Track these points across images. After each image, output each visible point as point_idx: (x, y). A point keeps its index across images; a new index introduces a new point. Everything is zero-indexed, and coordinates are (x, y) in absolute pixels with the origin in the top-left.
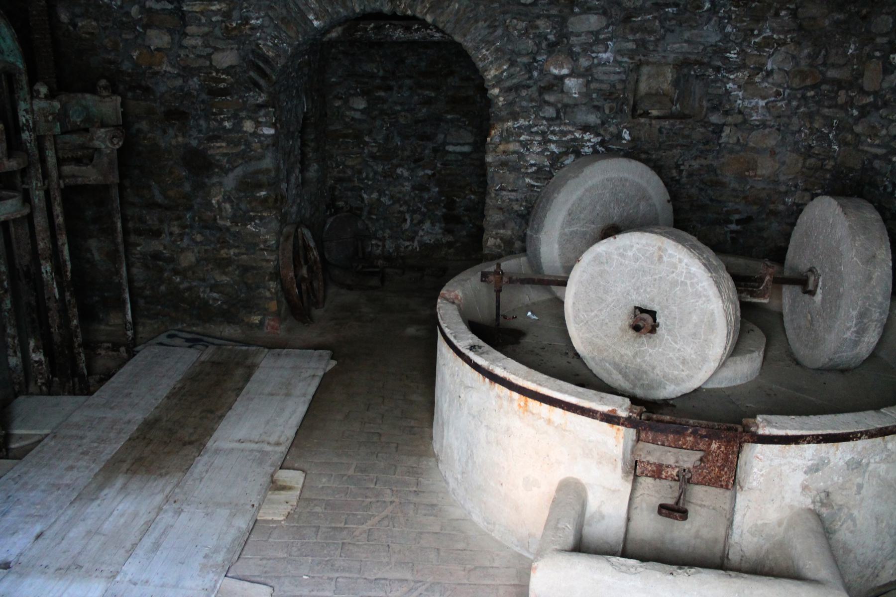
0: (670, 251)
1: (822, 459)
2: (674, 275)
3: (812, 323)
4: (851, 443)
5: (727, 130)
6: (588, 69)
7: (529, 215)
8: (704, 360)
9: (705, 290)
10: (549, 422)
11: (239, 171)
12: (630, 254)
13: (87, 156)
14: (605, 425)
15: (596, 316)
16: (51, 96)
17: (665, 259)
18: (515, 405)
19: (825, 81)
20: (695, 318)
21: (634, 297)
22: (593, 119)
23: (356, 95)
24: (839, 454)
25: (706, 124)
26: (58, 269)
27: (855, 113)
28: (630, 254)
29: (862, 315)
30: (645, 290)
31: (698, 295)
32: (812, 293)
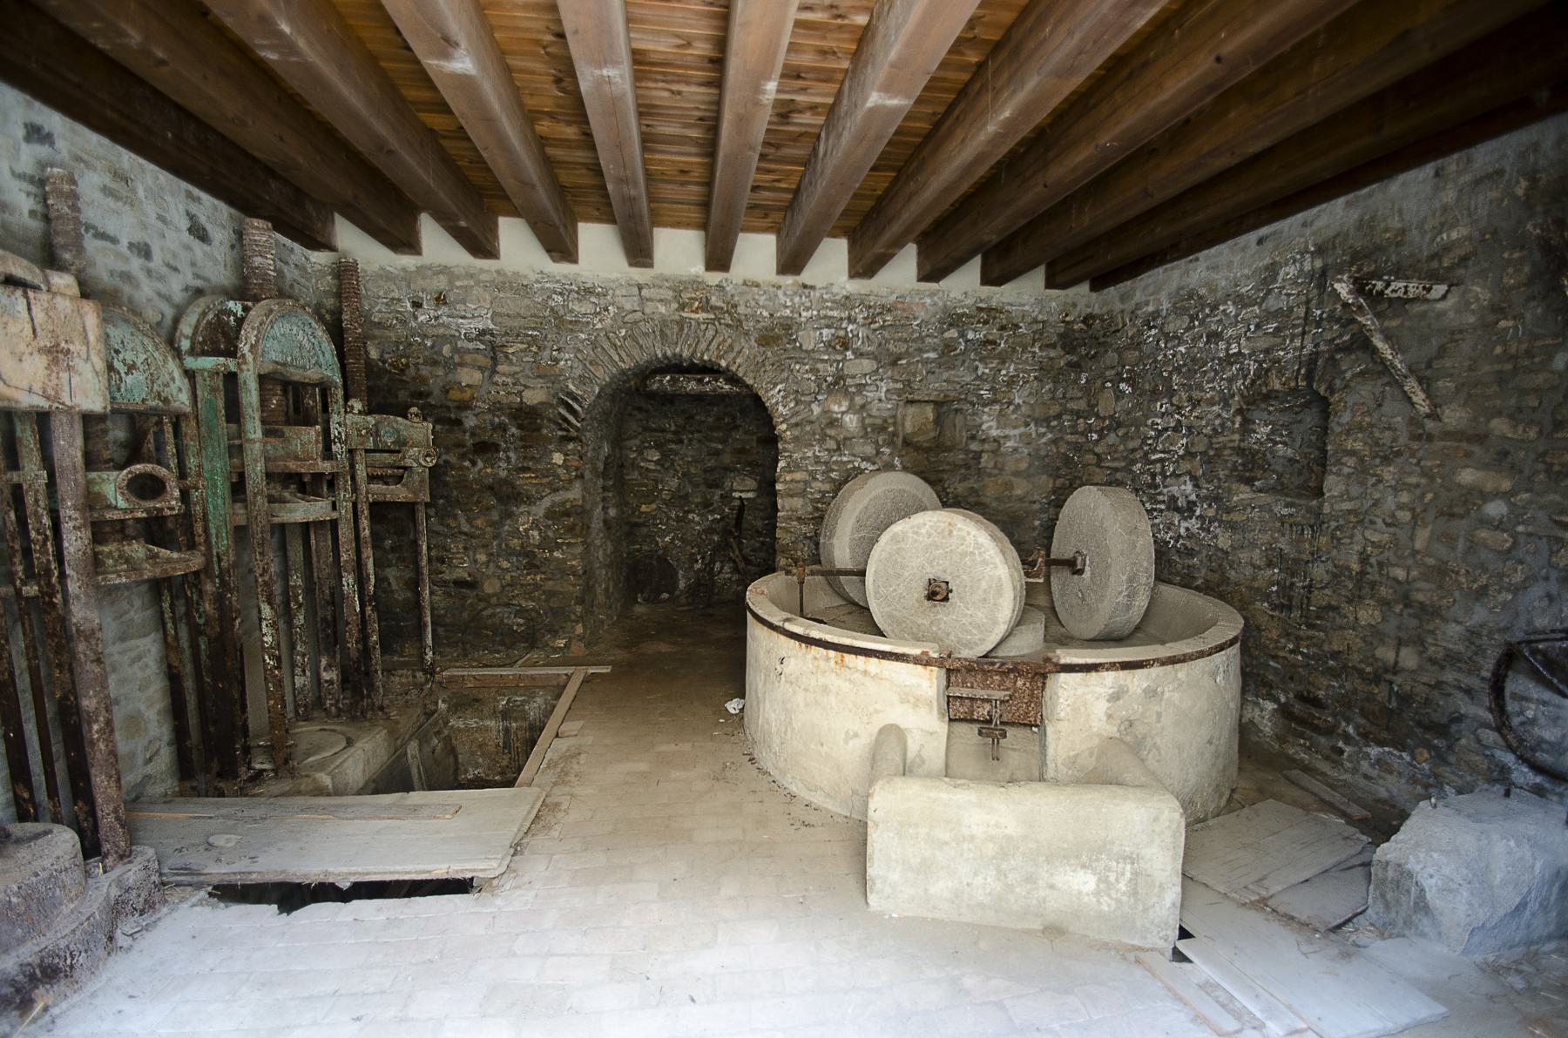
1: (1121, 687)
3: (1083, 599)
4: (1145, 671)
5: (985, 457)
6: (863, 407)
7: (819, 517)
8: (995, 623)
10: (865, 673)
11: (547, 502)
12: (923, 531)
13: (399, 475)
16: (369, 411)
19: (1065, 411)
20: (984, 584)
22: (869, 450)
23: (650, 447)
24: (1136, 681)
25: (967, 452)
26: (361, 581)
27: (1095, 437)
28: (923, 531)
29: (1131, 580)
31: (985, 563)
32: (1080, 572)
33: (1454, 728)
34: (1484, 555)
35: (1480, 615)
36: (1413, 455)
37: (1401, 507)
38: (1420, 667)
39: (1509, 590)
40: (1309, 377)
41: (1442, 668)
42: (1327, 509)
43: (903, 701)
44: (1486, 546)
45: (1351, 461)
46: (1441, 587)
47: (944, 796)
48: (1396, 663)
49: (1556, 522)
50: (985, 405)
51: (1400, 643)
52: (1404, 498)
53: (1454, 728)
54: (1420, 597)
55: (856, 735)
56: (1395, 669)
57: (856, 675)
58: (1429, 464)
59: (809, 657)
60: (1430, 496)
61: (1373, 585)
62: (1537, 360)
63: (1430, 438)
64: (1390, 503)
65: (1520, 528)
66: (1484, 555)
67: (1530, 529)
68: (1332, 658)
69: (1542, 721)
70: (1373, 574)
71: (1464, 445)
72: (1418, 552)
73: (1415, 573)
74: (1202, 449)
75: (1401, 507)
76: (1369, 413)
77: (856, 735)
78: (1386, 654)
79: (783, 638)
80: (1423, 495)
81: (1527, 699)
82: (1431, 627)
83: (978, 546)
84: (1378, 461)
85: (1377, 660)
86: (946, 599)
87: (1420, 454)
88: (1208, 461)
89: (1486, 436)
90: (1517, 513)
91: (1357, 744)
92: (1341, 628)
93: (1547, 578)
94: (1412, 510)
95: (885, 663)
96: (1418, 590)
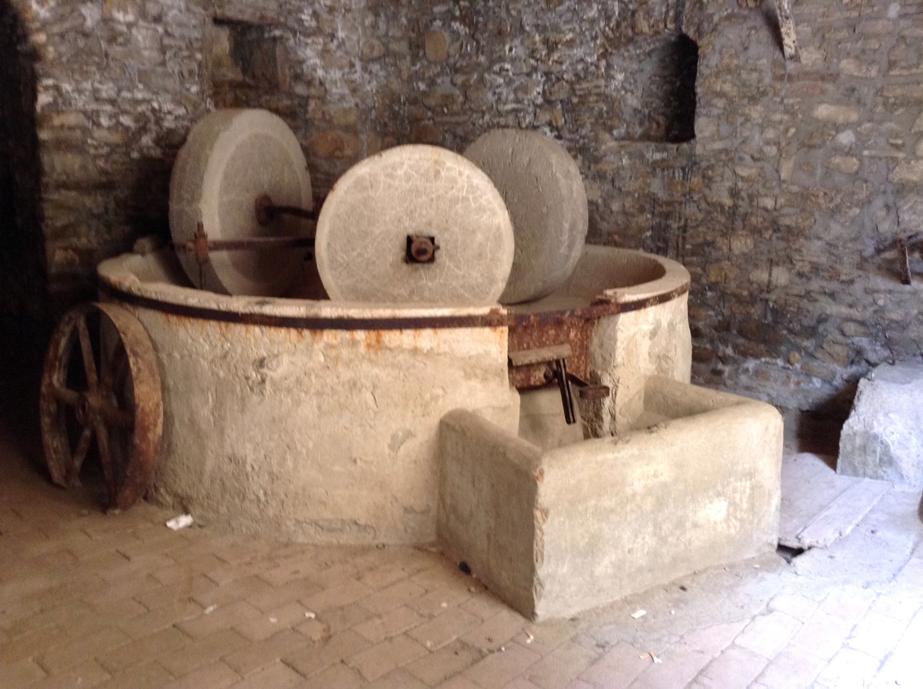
0: (448, 164)
2: (454, 191)
5: (312, 104)
8: (492, 281)
9: (489, 202)
14: (487, 330)
15: (360, 255)
17: (443, 174)
18: (362, 349)
21: (407, 224)
25: (291, 95)
28: (400, 172)
30: (421, 214)
31: (481, 210)
33: (821, 328)
34: (838, 178)
35: (836, 229)
36: (776, 94)
37: (767, 143)
38: (791, 282)
39: (857, 206)
40: (677, 19)
41: (809, 279)
42: (699, 150)
43: (468, 376)
44: (840, 172)
45: (721, 103)
46: (803, 210)
47: (610, 456)
48: (770, 282)
49: (892, 145)
50: (307, 35)
51: (772, 263)
52: (770, 134)
53: (821, 328)
54: (787, 221)
55: (409, 434)
56: (769, 287)
57: (401, 357)
58: (791, 101)
59: (319, 346)
60: (792, 130)
61: (745, 216)
62: (876, 9)
63: (790, 78)
64: (757, 139)
65: (866, 153)
66: (838, 178)
67: (874, 153)
68: (710, 289)
69: (890, 306)
70: (744, 207)
71: (820, 83)
72: (784, 181)
73: (781, 201)
74: (563, 95)
75: (767, 143)
76: (737, 55)
77: (409, 434)
78: (760, 276)
79: (256, 330)
80: (787, 130)
81: (877, 291)
82: (797, 246)
83: (472, 188)
84: (746, 101)
85: (751, 283)
86: (432, 260)
87: (783, 93)
88: (569, 108)
89: (838, 75)
90: (862, 141)
91: (735, 361)
92: (718, 260)
93: (884, 192)
94: (778, 144)
95: (446, 334)
96: (785, 216)
